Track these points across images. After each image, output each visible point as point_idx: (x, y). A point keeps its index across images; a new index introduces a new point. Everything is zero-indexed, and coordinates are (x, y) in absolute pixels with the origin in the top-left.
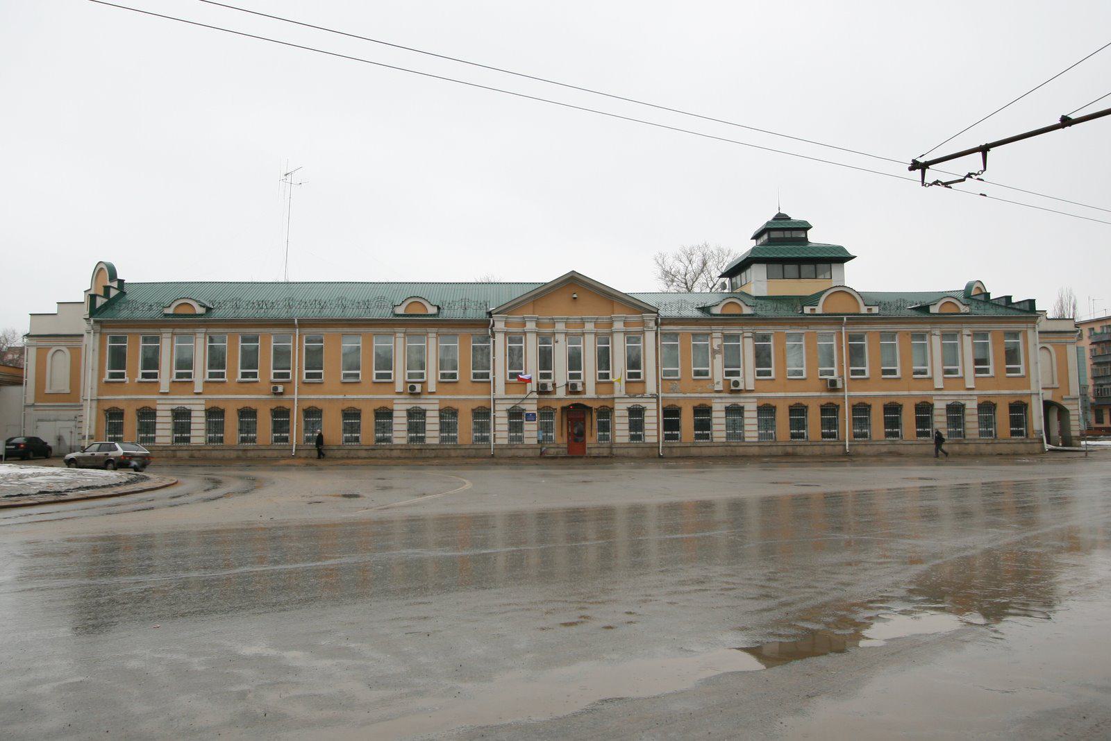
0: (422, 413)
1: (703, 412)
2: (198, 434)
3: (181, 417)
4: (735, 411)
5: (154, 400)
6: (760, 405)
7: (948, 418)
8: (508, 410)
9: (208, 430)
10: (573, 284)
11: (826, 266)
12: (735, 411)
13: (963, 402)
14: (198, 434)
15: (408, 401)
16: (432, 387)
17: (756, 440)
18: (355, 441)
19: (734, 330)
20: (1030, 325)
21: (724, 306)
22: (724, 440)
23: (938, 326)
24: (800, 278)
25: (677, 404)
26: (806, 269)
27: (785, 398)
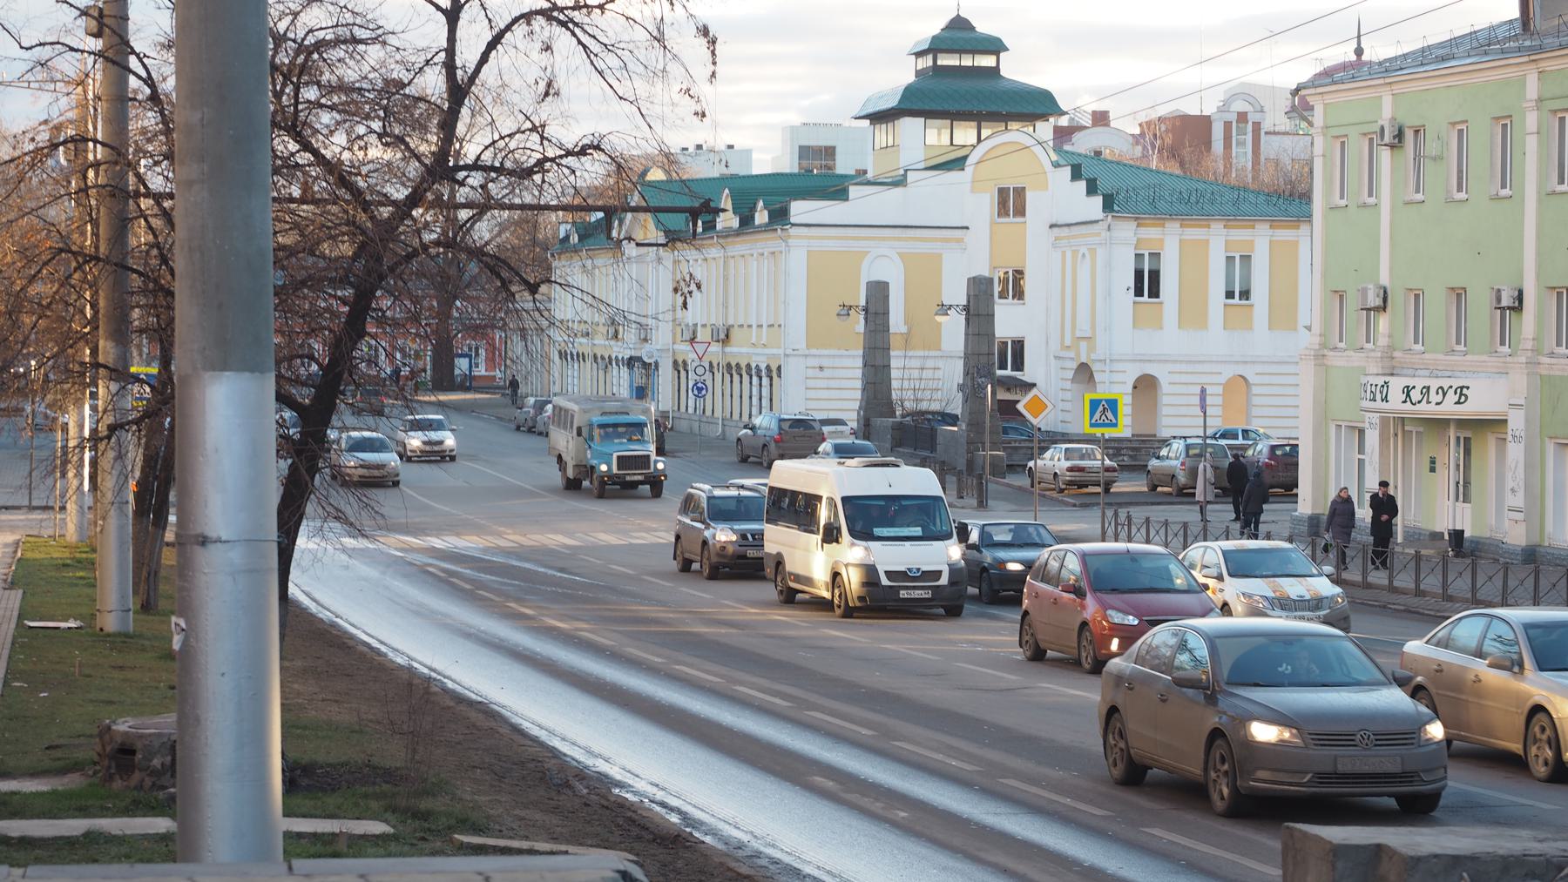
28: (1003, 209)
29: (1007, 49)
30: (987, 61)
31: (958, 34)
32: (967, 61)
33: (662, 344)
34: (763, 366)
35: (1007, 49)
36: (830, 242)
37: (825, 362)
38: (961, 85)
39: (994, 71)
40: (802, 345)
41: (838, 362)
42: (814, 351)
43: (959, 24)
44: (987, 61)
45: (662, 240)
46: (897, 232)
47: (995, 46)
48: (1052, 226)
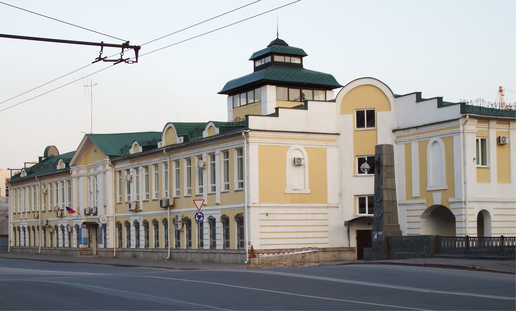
24: (247, 104)
28: (360, 123)
29: (306, 55)
30: (297, 61)
31: (278, 46)
32: (287, 59)
33: (108, 215)
34: (26, 226)
35: (306, 55)
36: (270, 140)
37: (269, 211)
38: (278, 68)
39: (300, 66)
40: (257, 201)
41: (276, 211)
42: (263, 204)
43: (278, 43)
44: (297, 61)
45: (180, 140)
46: (272, 134)
47: (301, 54)
48: (394, 131)
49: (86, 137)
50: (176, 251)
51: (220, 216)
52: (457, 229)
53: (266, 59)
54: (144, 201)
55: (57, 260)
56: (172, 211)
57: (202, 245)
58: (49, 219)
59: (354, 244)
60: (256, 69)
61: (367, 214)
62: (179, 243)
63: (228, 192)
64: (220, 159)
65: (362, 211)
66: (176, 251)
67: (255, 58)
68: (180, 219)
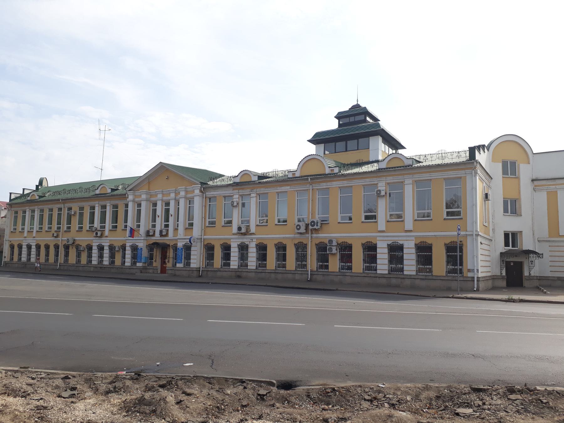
0: (247, 247)
1: (226, 248)
2: (410, 265)
3: (396, 251)
4: (243, 248)
5: (230, 239)
6: (417, 243)
7: (418, 256)
8: (97, 246)
9: (418, 262)
10: (163, 171)
11: (365, 139)
12: (243, 248)
13: (401, 242)
14: (410, 265)
15: (239, 238)
16: (253, 229)
17: (386, 272)
18: (347, 269)
19: (247, 192)
20: (468, 171)
21: (242, 176)
22: (414, 273)
23: (384, 178)
24: (346, 151)
25: (427, 241)
26: (352, 144)
27: (273, 239)
48: (533, 180)
49: (161, 165)
50: (316, 273)
51: (35, 244)
52: (404, 261)
53: (351, 118)
54: (37, 231)
55: (325, 288)
56: (314, 235)
57: (90, 261)
58: (76, 239)
59: (504, 273)
60: (340, 125)
61: (510, 248)
62: (13, 258)
63: (351, 223)
64: (20, 215)
65: (507, 244)
66: (316, 273)
67: (339, 116)
68: (335, 243)
